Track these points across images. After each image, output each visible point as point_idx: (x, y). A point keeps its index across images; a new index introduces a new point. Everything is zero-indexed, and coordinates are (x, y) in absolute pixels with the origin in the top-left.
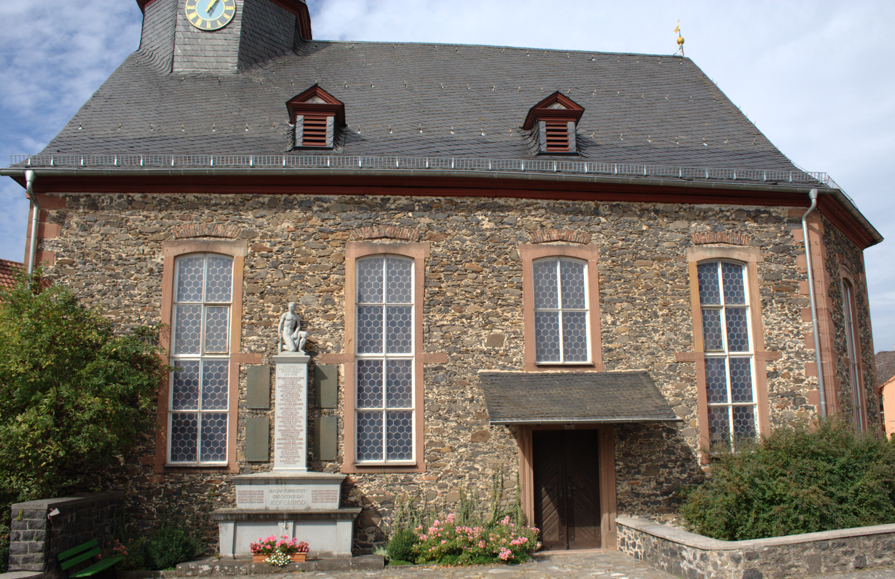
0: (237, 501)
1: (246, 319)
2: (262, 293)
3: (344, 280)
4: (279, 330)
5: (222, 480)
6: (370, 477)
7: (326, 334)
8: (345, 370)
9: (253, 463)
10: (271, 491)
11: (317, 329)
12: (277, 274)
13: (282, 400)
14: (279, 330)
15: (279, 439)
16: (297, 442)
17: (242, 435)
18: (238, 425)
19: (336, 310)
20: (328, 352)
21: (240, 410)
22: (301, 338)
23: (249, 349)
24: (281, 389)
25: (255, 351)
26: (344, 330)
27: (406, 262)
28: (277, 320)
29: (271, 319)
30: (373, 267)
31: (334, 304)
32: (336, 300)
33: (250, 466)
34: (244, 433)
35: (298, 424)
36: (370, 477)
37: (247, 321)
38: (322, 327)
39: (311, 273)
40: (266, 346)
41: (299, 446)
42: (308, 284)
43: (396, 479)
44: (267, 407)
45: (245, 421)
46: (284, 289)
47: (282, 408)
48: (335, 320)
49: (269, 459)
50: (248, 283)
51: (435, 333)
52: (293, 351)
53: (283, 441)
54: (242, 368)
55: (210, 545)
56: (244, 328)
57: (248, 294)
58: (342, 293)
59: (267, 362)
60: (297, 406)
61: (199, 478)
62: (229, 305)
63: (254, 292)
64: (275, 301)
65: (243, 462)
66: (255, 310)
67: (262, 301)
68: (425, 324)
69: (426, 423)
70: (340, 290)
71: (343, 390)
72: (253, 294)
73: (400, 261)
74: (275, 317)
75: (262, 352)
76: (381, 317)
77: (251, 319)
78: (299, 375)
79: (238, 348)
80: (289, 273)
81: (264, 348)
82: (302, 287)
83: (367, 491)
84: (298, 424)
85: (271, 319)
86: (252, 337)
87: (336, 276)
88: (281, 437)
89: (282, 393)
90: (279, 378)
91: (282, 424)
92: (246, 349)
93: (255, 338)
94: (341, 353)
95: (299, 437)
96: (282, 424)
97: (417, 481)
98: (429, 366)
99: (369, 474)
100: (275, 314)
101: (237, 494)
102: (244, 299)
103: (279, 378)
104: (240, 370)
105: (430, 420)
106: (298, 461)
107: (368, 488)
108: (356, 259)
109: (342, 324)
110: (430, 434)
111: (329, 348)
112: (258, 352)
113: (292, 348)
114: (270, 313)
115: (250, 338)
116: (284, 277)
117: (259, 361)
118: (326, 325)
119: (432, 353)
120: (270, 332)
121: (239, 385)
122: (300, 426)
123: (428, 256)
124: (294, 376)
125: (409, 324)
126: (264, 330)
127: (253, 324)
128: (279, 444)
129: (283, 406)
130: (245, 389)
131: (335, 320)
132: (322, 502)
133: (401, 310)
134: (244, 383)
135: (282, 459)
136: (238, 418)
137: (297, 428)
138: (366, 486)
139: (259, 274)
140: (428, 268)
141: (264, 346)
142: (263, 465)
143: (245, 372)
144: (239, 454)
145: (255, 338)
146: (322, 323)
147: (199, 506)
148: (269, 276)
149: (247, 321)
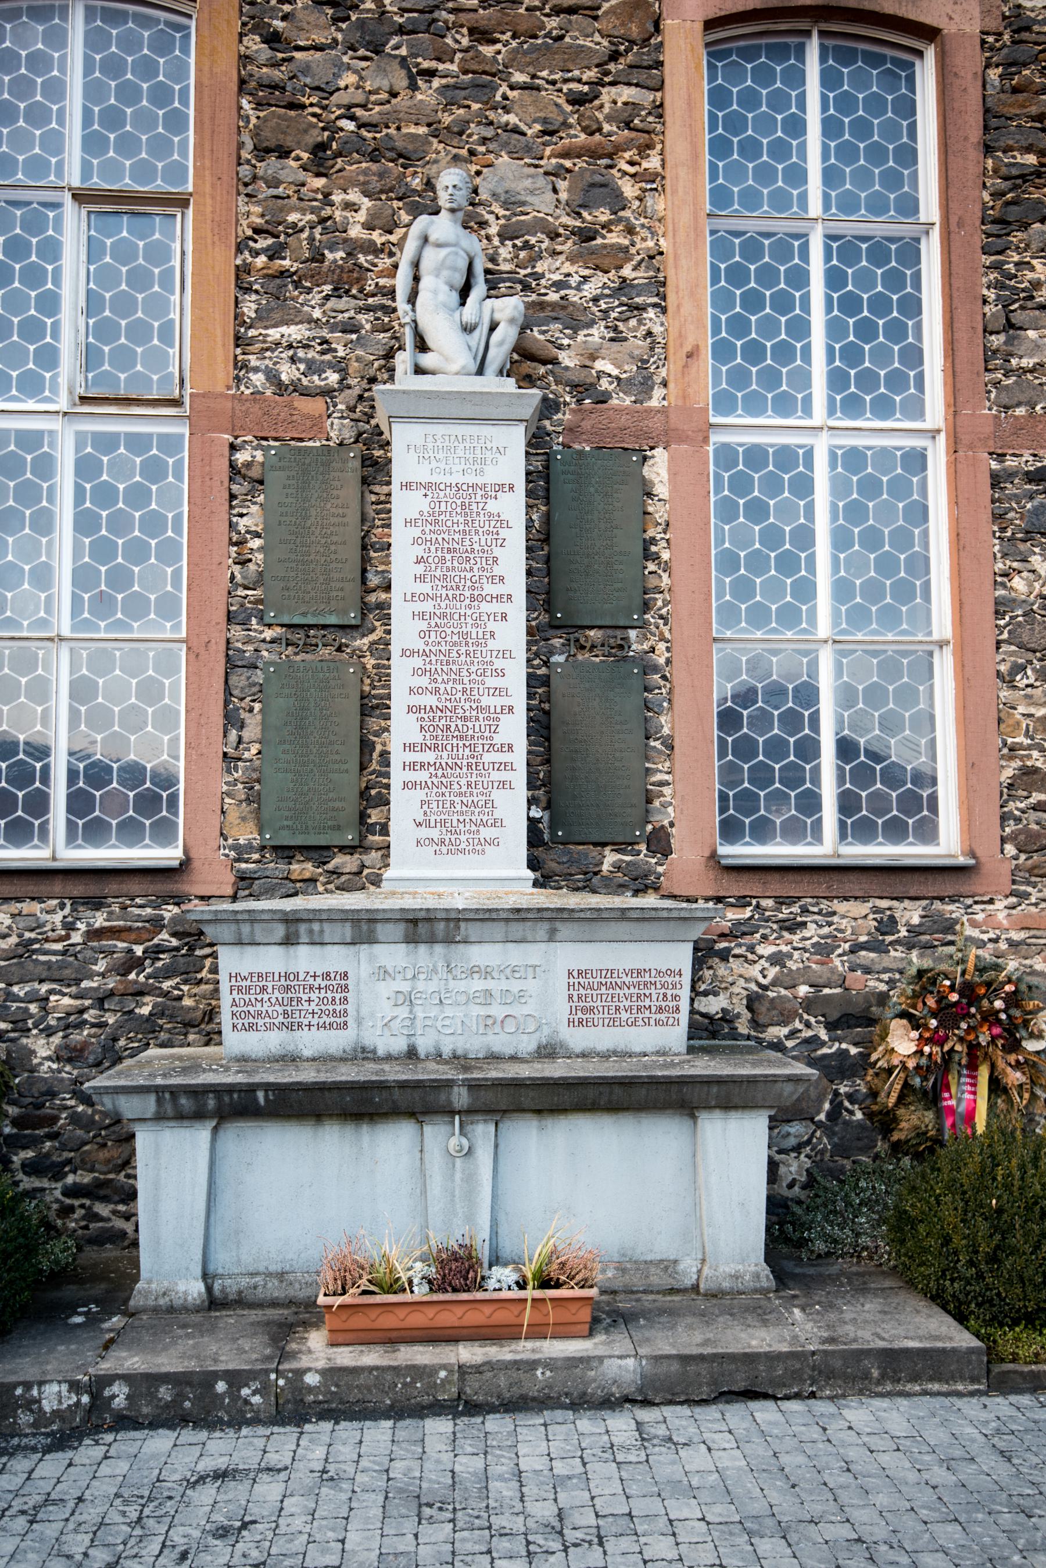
0: (226, 1019)
1: (256, 253)
2: (320, 147)
3: (658, 110)
4: (401, 294)
5: (157, 924)
6: (785, 912)
7: (591, 324)
8: (673, 474)
9: (286, 852)
10: (384, 974)
11: (553, 305)
12: (382, 71)
13: (422, 579)
14: (401, 294)
15: (411, 747)
16: (488, 758)
17: (246, 734)
18: (228, 692)
19: (630, 230)
20: (603, 399)
21: (237, 632)
22: (493, 327)
23: (273, 377)
24: (416, 532)
25: (296, 387)
26: (664, 310)
27: (895, 61)
28: (384, 262)
29: (362, 259)
30: (764, 76)
31: (618, 203)
32: (629, 189)
33: (275, 867)
34: (252, 730)
35: (491, 682)
36: (785, 912)
37: (261, 260)
38: (574, 297)
39: (519, 77)
40: (341, 367)
41: (496, 776)
42: (512, 119)
43: (888, 925)
44: (352, 617)
45: (259, 677)
46: (414, 137)
47: (422, 615)
48: (627, 271)
49: (362, 837)
50: (259, 105)
51: (1031, 334)
52: (463, 372)
53: (429, 757)
54: (242, 457)
55: (103, 1209)
56: (248, 290)
57: (262, 151)
58: (653, 163)
59: (349, 435)
60: (486, 607)
61: (58, 918)
62: (183, 203)
63: (289, 142)
64: (375, 185)
65: (250, 848)
66: (293, 217)
67: (320, 182)
68: (991, 295)
69: (1005, 694)
70: (644, 149)
71: (665, 556)
72: (284, 153)
73: (875, 60)
74: (376, 251)
75: (327, 392)
76: (800, 278)
77: (274, 254)
78: (492, 475)
79: (224, 373)
80: (431, 73)
81: (333, 378)
82: (489, 132)
83: (773, 972)
84: (491, 682)
85: (362, 259)
86: (284, 329)
87: (626, 94)
88: (417, 738)
89: (419, 551)
90: (407, 486)
91: (424, 681)
92: (258, 379)
93: (295, 332)
94: (654, 403)
95: (498, 739)
96: (424, 681)
97: (975, 933)
98: (1011, 463)
99: (782, 901)
100: (378, 237)
101: (224, 987)
102: (245, 171)
103: (407, 486)
104: (232, 465)
105: (1021, 681)
106: (492, 842)
107: (777, 959)
108: (710, 25)
109: (659, 286)
110: (1021, 739)
111: (604, 384)
112: (306, 393)
113: (465, 360)
114: (355, 232)
115: (274, 334)
116: (413, 87)
117: (316, 424)
118: (590, 289)
119: (1021, 411)
120: (360, 310)
121: (232, 526)
122: (498, 691)
123: (994, 24)
124: (471, 479)
125: (913, 306)
126: (332, 303)
127: (283, 274)
128: (412, 766)
129: (428, 606)
130: (256, 543)
131: (627, 271)
132: (613, 1023)
133: (879, 252)
134: (252, 519)
135: (424, 833)
136: (231, 665)
137: (485, 701)
138: (765, 950)
139: (306, 69)
140: (994, 74)
141: (331, 366)
142: (339, 861)
143: (255, 473)
144: (233, 815)
145: (295, 332)
146: (574, 281)
147: (57, 1039)
148: (349, 79)
149: (261, 260)
